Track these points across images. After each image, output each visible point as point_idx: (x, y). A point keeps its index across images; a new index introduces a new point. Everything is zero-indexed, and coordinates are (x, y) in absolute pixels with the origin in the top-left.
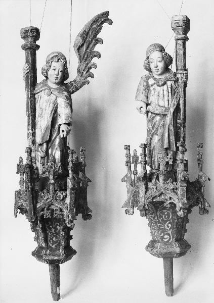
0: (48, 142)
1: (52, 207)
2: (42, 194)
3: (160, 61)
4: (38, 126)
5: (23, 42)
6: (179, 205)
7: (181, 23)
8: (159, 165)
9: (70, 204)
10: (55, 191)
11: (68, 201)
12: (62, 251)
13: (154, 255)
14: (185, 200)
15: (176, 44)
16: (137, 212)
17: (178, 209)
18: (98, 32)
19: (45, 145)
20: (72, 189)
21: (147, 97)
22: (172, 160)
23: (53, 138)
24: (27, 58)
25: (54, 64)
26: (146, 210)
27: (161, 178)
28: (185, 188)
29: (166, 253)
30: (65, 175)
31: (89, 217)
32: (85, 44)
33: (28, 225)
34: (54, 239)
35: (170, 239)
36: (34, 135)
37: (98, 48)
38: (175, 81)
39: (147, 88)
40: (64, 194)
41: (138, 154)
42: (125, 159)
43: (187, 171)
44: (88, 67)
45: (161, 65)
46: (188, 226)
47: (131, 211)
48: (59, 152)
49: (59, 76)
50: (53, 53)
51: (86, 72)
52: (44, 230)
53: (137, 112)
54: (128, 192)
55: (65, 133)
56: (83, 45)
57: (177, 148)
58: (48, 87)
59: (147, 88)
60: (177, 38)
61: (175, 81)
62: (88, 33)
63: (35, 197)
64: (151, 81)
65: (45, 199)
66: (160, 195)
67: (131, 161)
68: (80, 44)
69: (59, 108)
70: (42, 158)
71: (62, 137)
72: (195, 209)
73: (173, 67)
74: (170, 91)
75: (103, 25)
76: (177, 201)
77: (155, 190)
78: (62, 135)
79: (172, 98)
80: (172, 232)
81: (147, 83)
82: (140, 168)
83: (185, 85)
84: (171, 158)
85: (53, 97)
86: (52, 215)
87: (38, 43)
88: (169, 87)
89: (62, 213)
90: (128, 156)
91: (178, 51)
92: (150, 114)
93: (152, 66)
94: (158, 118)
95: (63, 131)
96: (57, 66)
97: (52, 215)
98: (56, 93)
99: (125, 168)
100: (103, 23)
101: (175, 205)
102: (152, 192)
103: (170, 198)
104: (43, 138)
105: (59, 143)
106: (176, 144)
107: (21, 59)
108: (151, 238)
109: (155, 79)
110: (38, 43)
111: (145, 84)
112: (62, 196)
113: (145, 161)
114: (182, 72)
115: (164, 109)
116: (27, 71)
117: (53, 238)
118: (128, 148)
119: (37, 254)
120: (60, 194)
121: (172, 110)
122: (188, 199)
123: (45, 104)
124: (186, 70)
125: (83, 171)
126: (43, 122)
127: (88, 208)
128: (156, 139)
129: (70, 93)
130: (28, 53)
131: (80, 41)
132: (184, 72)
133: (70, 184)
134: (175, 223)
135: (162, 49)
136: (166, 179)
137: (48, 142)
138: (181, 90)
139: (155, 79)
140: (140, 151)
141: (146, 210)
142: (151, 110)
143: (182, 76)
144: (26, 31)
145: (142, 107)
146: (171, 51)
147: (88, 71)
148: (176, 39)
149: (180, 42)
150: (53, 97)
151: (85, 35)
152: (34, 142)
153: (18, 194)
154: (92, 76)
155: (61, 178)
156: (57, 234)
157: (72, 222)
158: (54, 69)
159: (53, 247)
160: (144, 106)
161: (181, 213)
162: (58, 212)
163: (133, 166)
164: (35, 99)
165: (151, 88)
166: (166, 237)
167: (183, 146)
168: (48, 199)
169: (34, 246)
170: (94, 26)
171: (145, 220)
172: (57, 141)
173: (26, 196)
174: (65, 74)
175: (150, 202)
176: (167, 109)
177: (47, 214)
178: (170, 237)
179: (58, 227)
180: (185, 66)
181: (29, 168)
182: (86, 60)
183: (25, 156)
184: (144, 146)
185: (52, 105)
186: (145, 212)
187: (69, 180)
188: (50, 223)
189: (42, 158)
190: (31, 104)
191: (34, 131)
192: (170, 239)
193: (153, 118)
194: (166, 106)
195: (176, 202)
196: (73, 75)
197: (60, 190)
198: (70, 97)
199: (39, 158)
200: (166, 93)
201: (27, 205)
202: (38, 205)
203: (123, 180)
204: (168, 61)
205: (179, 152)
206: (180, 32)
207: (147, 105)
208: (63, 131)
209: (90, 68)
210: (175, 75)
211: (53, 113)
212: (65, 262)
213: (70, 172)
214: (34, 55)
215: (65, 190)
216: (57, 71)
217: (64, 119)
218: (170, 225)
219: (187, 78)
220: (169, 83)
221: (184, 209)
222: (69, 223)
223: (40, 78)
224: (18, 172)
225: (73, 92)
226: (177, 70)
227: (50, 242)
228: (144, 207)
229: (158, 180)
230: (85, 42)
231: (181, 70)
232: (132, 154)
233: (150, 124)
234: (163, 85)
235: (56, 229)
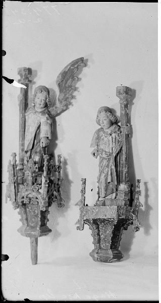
36: (23, 145)
81: (98, 135)
112: (37, 188)
126: (30, 136)
152: (23, 150)
156: (36, 216)
188: (30, 208)
235: (34, 212)
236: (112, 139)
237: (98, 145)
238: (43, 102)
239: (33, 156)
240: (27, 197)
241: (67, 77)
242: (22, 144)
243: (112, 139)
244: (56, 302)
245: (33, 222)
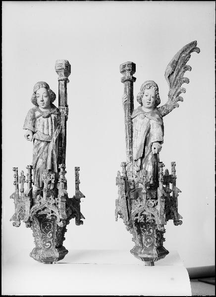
1: (144, 213)
2: (136, 202)
3: (46, 97)
4: (134, 146)
5: (122, 76)
6: (59, 217)
7: (64, 66)
8: (43, 184)
9: (160, 211)
10: (147, 199)
11: (158, 208)
12: (155, 251)
13: (36, 259)
14: (65, 213)
15: (59, 84)
16: (23, 224)
17: (58, 220)
18: (187, 60)
19: (139, 160)
20: (162, 197)
21: (34, 127)
22: (54, 179)
23: (146, 155)
24: (125, 89)
25: (146, 91)
26: (31, 222)
27: (45, 194)
28: (65, 203)
29: (47, 258)
31: (181, 223)
32: (175, 72)
33: (125, 227)
35: (51, 246)
36: (131, 153)
37: (187, 74)
38: (57, 114)
39: (34, 119)
40: (155, 202)
41: (25, 174)
42: (14, 180)
43: (66, 189)
44: (178, 91)
45: (46, 100)
46: (66, 235)
47: (18, 223)
48: (152, 167)
49: (151, 101)
50: (146, 82)
51: (177, 97)
52: (139, 232)
53: (25, 139)
54: (16, 207)
56: (173, 73)
57: (59, 170)
58: (142, 111)
59: (34, 119)
60: (60, 79)
61: (57, 114)
62: (177, 62)
63: (129, 202)
64: (37, 114)
65: (136, 208)
66: (43, 209)
67: (17, 181)
68: (170, 72)
70: (137, 171)
71: (154, 153)
72: (73, 221)
73: (56, 103)
74: (53, 123)
75: (191, 54)
76: (57, 213)
77: (39, 204)
78: (154, 151)
79: (55, 129)
80: (53, 240)
81: (34, 115)
82: (26, 187)
83: (66, 119)
84: (53, 178)
85: (146, 120)
86: (145, 220)
87: (134, 75)
88: (53, 118)
90: (16, 176)
91: (60, 89)
92: (36, 141)
93: (39, 100)
94: (43, 144)
96: (151, 92)
98: (149, 116)
99: (14, 187)
100: (191, 51)
101: (56, 217)
102: (37, 206)
103: (52, 212)
104: (137, 155)
105: (151, 158)
106: (58, 166)
107: (121, 90)
108: (34, 246)
109: (41, 112)
110: (134, 75)
111: (32, 115)
112: (153, 204)
113: (31, 180)
114: (63, 108)
115: (48, 137)
116: (125, 100)
118: (15, 170)
119: (134, 252)
120: (152, 202)
121: (55, 138)
122: (67, 212)
123: (140, 126)
124: (67, 106)
125: (174, 184)
126: (138, 141)
127: (178, 215)
128: (40, 161)
129: (162, 117)
130: (126, 85)
131: (170, 70)
132: (66, 108)
133: (160, 194)
134: (55, 233)
135: (47, 87)
137: (142, 158)
138: (62, 123)
139: (41, 112)
140: (26, 172)
141: (31, 222)
142: (37, 138)
143: (64, 110)
144: (124, 66)
145: (29, 135)
146: (55, 88)
147: (178, 96)
148: (59, 81)
149: (63, 82)
150: (146, 120)
151: (174, 64)
152: (131, 159)
153: (117, 201)
154: (181, 100)
155: (153, 187)
156: (151, 236)
157: (163, 226)
159: (148, 247)
160: (31, 134)
161: (61, 224)
162: (150, 218)
163: (20, 185)
164: (132, 123)
165: (38, 119)
166: (47, 244)
167: (64, 168)
168: (141, 206)
169: (133, 245)
170: (183, 55)
171: (30, 231)
172: (150, 157)
173: (123, 202)
174: (157, 102)
175: (35, 215)
176: (51, 138)
177: (141, 219)
178: (51, 243)
179: (151, 231)
180: (66, 102)
181: (124, 179)
182: (176, 86)
183: (121, 169)
184: (30, 167)
185: (145, 127)
186: (30, 223)
187: (158, 190)
188: (144, 226)
189: (137, 171)
190: (129, 127)
191: (131, 150)
192: (51, 246)
193: (39, 144)
194: (50, 135)
195: (57, 214)
196: (164, 100)
197: (152, 199)
198: (162, 119)
199: (136, 172)
200: (50, 124)
201: (125, 213)
202: (133, 211)
203: (12, 197)
204: (51, 96)
205: (60, 173)
206: (63, 74)
207: (34, 133)
208: (155, 148)
209: (180, 93)
210: (58, 110)
212: (157, 260)
213: (160, 183)
214: (132, 85)
215: (156, 199)
216: (149, 97)
217: (155, 138)
218: (51, 235)
219: (67, 113)
220: (53, 116)
221: (63, 220)
222: (159, 228)
223: (136, 105)
224: (117, 184)
225: (165, 115)
226: (59, 105)
228: (29, 219)
229: (42, 196)
231: (63, 106)
232: (20, 175)
233: (36, 149)
234: (48, 117)
235: (150, 232)
236: (52, 121)
237: (34, 127)
238: (152, 100)
239: (144, 166)
240: (141, 215)
241: (178, 67)
242: (130, 152)
243: (52, 121)
244: (9, 296)
245: (148, 243)
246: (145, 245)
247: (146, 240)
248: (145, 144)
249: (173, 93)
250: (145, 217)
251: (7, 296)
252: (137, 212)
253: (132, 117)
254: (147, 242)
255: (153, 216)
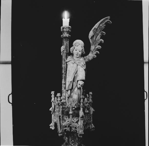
0: (71, 90)
1: (71, 126)
3: (79, 89)
4: (67, 80)
19: (69, 91)
23: (74, 87)
30: (78, 109)
34: (73, 141)
55: (80, 86)
69: (78, 72)
86: (71, 130)
89: (76, 129)
95: (79, 84)
97: (71, 130)
117: (72, 140)
136: (73, 117)
137: (71, 90)
158: (76, 50)
162: (74, 129)
164: (67, 65)
170: (101, 25)
211: (74, 74)
215: (110, 20)
227: (71, 142)
230: (95, 34)
235: (74, 136)
246: (71, 143)
247: (72, 140)
248: (74, 81)
249: (93, 49)
250: (71, 128)
251: (148, 57)
252: (66, 125)
253: (67, 61)
254: (72, 142)
255: (76, 128)
